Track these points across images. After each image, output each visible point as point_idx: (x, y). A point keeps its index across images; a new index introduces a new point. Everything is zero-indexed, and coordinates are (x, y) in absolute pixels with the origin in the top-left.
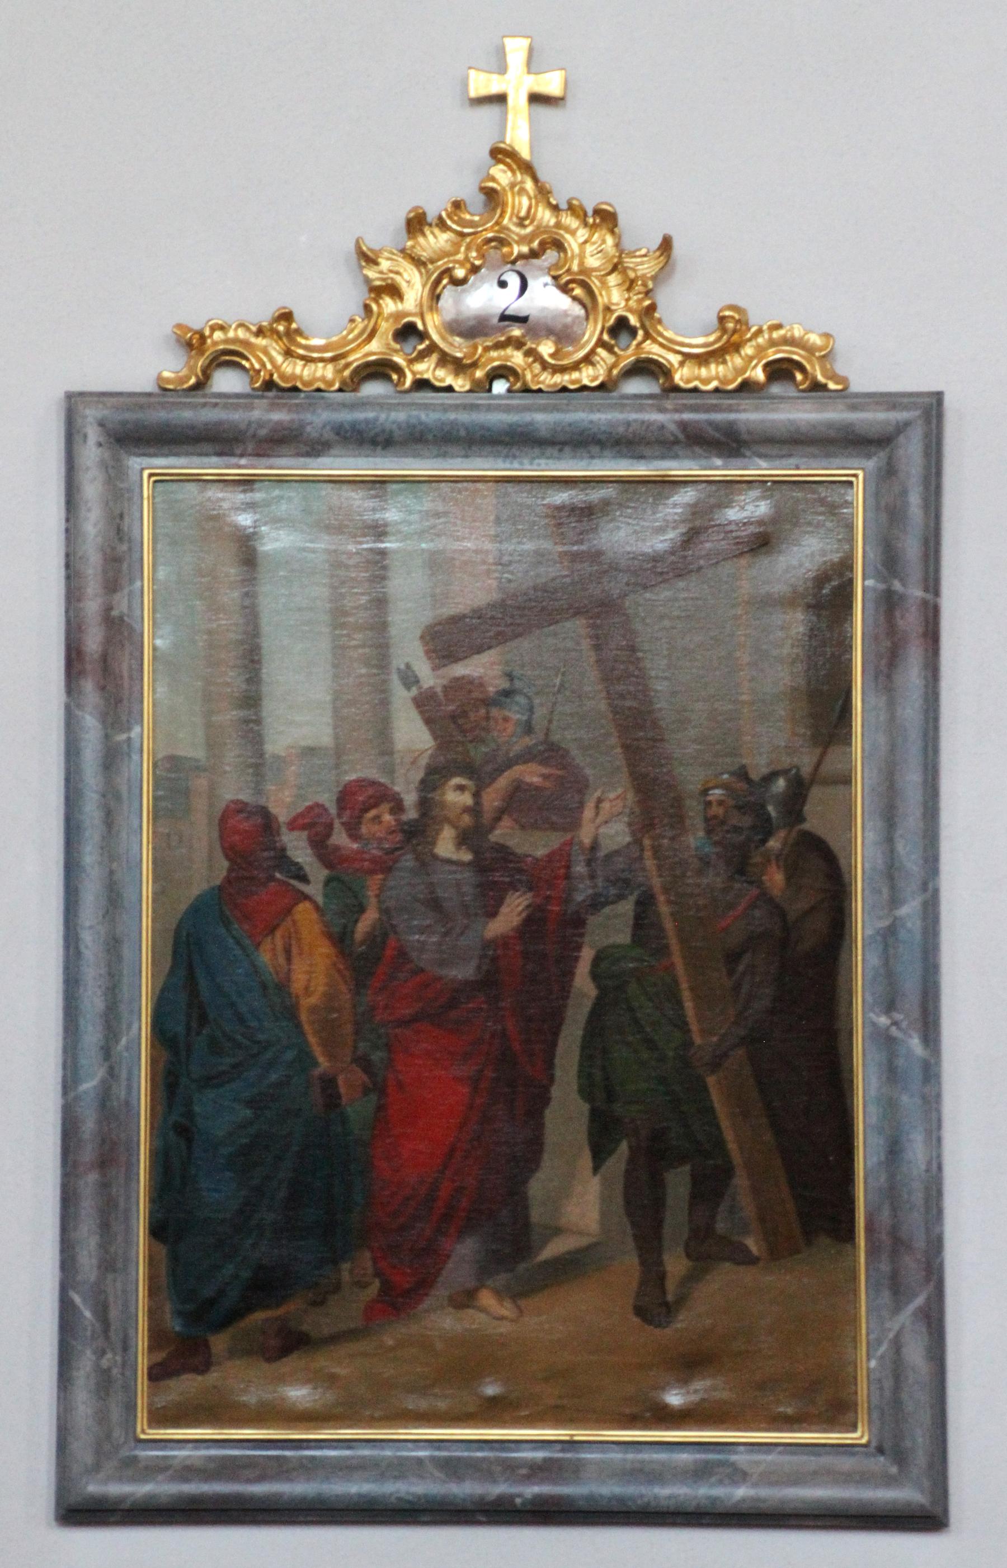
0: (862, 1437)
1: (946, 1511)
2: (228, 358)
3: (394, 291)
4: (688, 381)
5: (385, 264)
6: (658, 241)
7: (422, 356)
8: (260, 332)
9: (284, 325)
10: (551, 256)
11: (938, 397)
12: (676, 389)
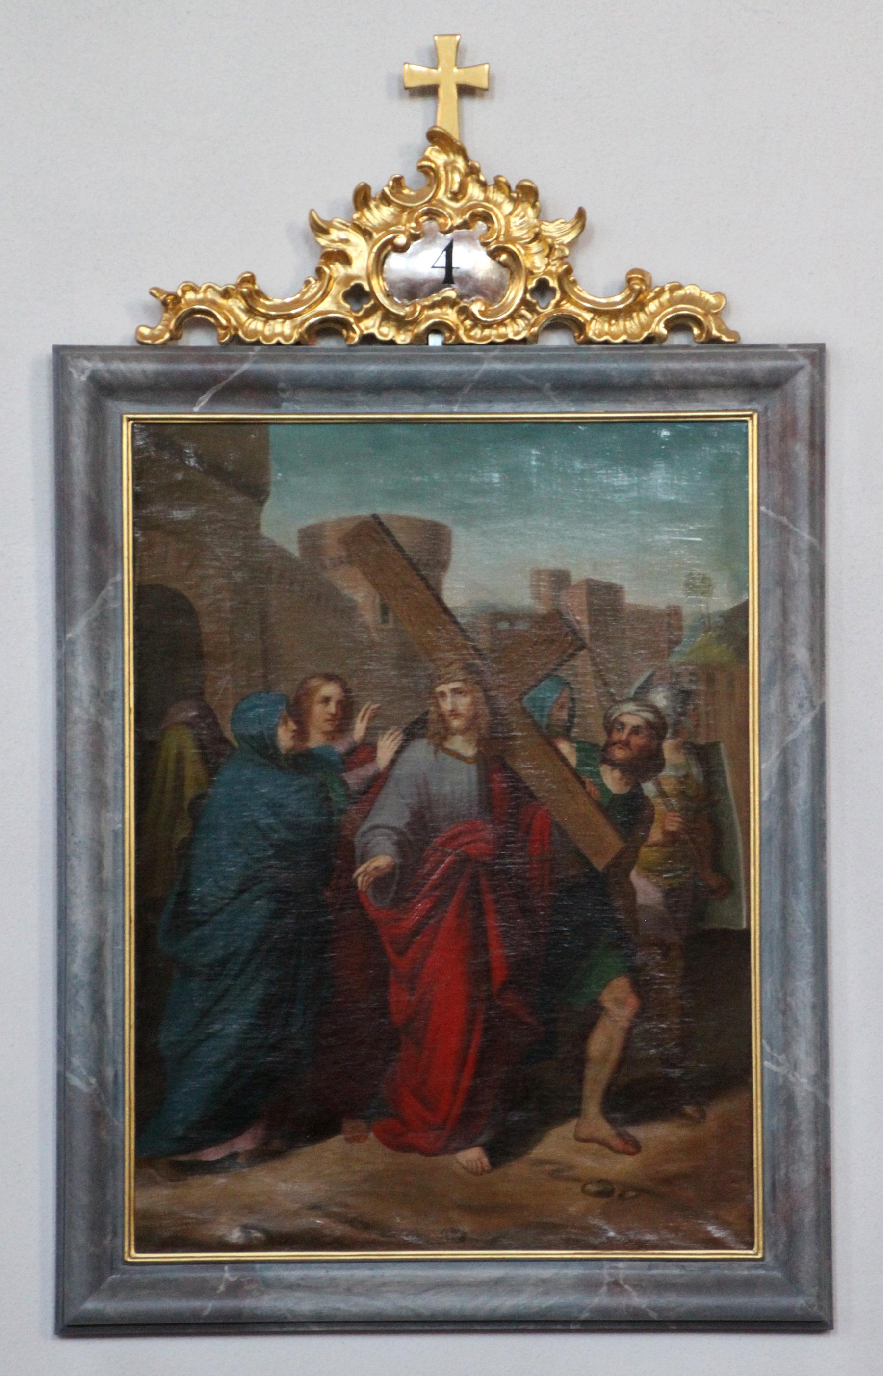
0: (757, 1254)
1: (832, 1321)
2: (194, 319)
4: (600, 336)
5: (334, 234)
6: (573, 213)
7: (368, 314)
9: (250, 294)
12: (590, 342)
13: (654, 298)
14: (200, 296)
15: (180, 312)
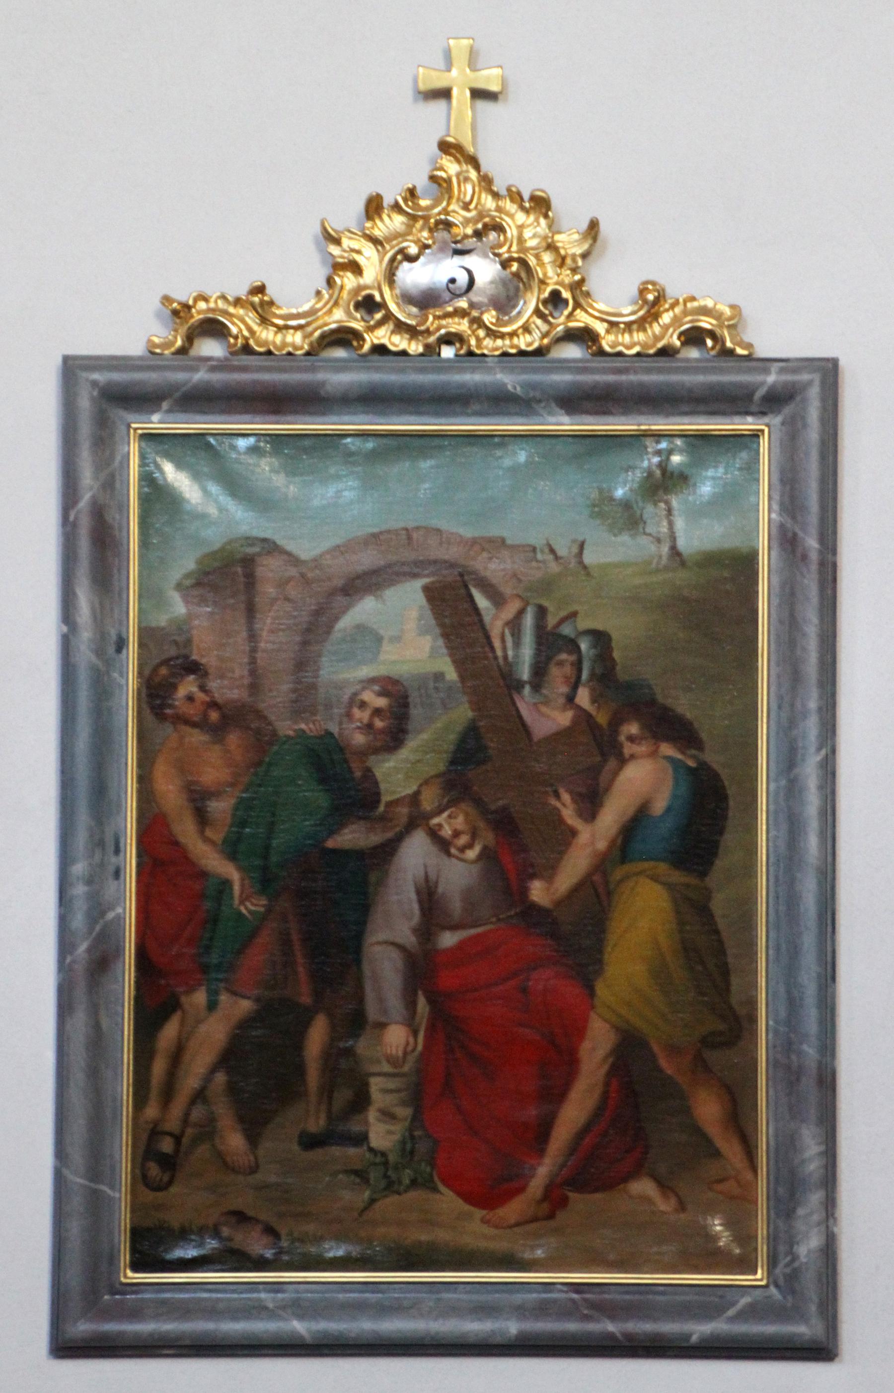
2: (212, 327)
5: (346, 243)
6: (584, 225)
7: (380, 323)
8: (237, 302)
9: (259, 301)
11: (835, 362)
12: (601, 353)
13: (667, 310)
15: (192, 321)
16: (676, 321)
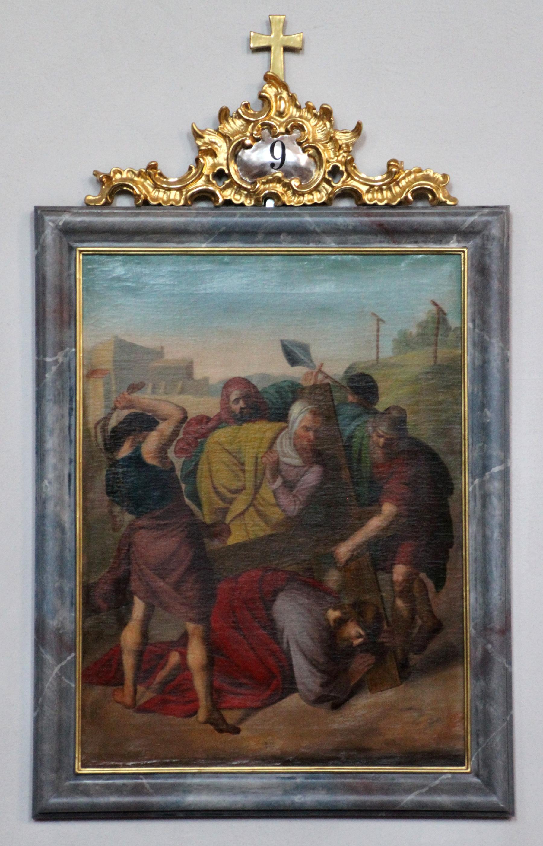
0: (467, 769)
2: (121, 190)
3: (214, 154)
4: (370, 201)
5: (207, 138)
8: (140, 174)
9: (151, 171)
10: (296, 134)
12: (365, 204)
13: (404, 178)
14: (124, 175)
16: (409, 184)
